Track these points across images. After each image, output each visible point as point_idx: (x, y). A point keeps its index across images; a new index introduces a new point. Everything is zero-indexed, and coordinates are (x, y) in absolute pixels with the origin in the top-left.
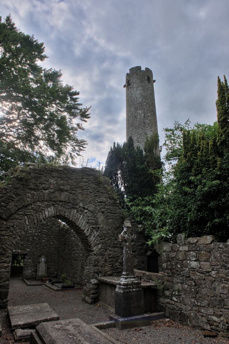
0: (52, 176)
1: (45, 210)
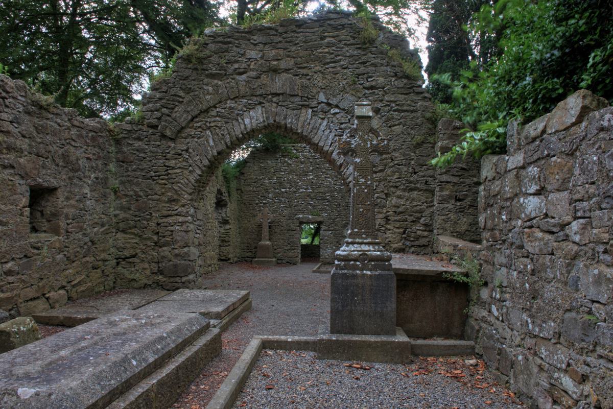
0: (252, 43)
1: (244, 115)
